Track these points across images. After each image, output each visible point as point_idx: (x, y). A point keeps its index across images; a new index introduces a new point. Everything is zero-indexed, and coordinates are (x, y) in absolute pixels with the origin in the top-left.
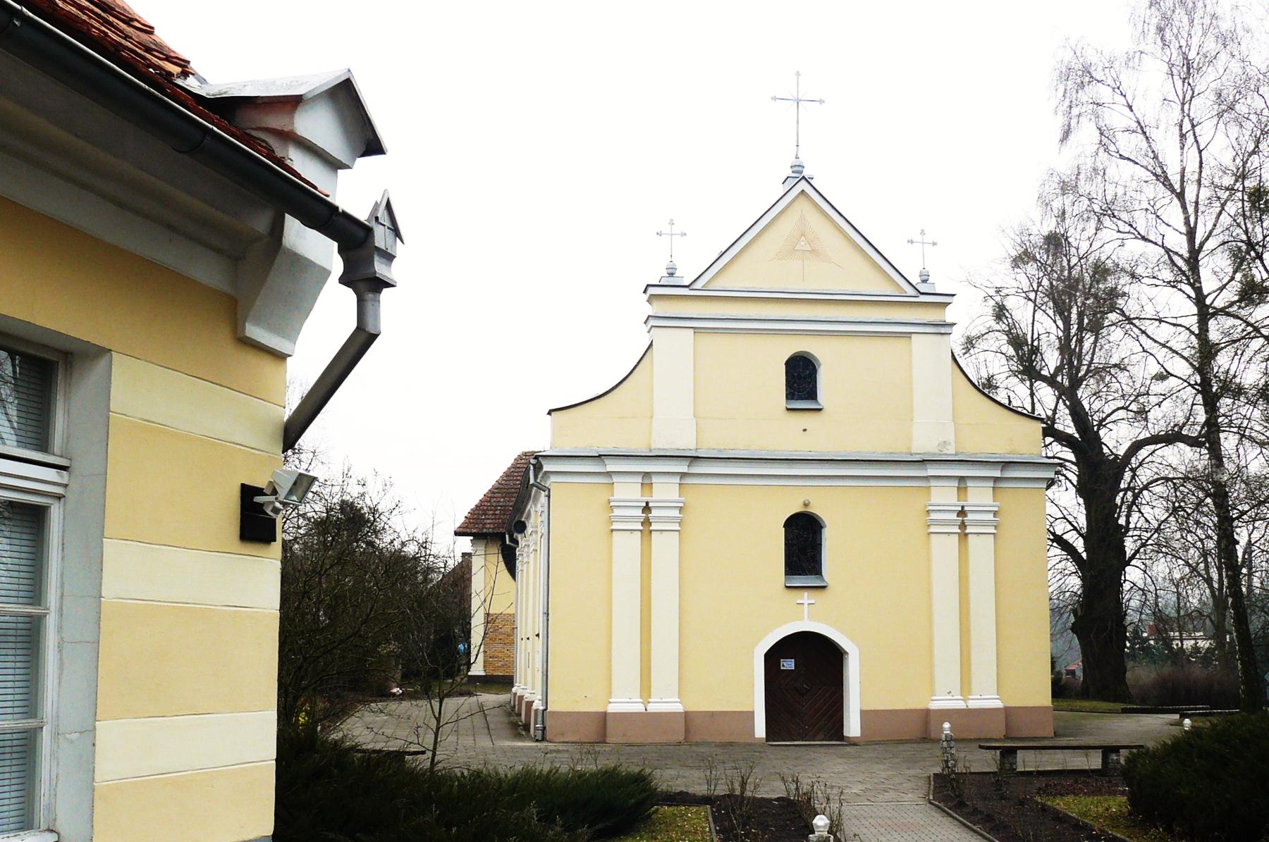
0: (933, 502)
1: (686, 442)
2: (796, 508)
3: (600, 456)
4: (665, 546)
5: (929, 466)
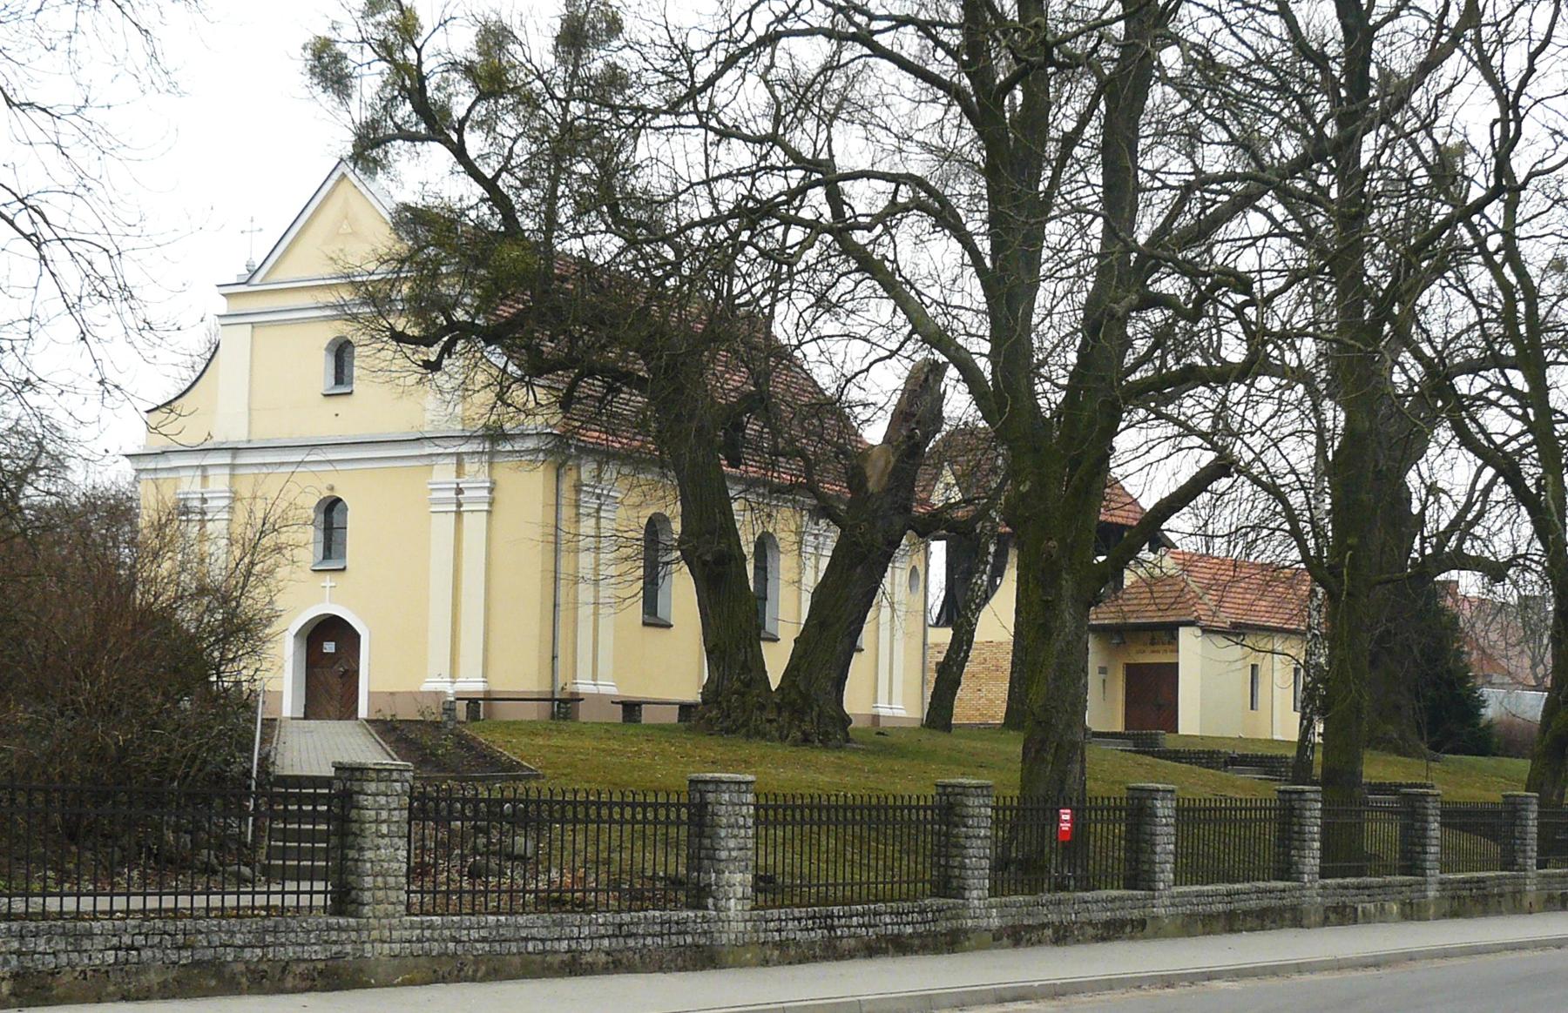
0: (434, 480)
1: (238, 436)
2: (326, 493)
3: (164, 453)
4: (475, 524)
5: (171, 456)
